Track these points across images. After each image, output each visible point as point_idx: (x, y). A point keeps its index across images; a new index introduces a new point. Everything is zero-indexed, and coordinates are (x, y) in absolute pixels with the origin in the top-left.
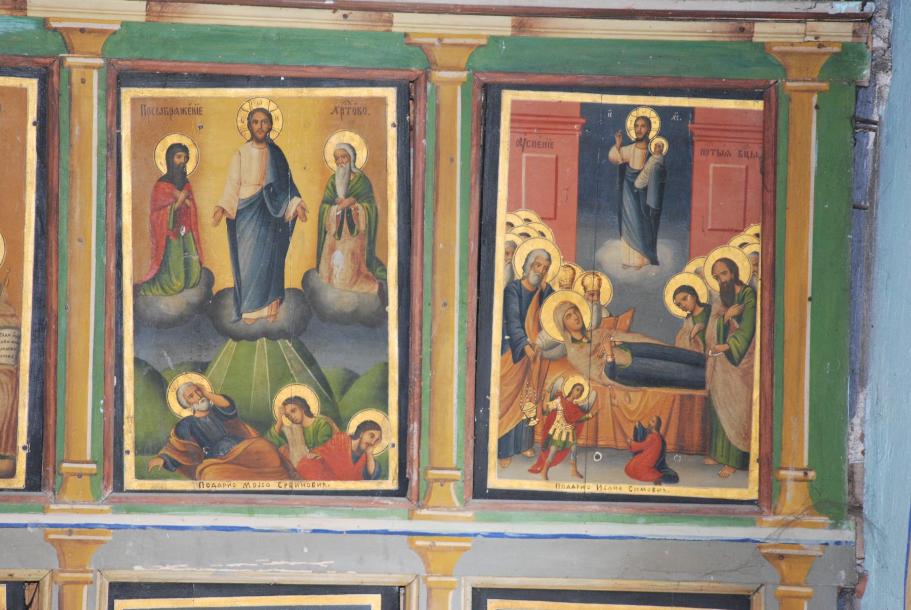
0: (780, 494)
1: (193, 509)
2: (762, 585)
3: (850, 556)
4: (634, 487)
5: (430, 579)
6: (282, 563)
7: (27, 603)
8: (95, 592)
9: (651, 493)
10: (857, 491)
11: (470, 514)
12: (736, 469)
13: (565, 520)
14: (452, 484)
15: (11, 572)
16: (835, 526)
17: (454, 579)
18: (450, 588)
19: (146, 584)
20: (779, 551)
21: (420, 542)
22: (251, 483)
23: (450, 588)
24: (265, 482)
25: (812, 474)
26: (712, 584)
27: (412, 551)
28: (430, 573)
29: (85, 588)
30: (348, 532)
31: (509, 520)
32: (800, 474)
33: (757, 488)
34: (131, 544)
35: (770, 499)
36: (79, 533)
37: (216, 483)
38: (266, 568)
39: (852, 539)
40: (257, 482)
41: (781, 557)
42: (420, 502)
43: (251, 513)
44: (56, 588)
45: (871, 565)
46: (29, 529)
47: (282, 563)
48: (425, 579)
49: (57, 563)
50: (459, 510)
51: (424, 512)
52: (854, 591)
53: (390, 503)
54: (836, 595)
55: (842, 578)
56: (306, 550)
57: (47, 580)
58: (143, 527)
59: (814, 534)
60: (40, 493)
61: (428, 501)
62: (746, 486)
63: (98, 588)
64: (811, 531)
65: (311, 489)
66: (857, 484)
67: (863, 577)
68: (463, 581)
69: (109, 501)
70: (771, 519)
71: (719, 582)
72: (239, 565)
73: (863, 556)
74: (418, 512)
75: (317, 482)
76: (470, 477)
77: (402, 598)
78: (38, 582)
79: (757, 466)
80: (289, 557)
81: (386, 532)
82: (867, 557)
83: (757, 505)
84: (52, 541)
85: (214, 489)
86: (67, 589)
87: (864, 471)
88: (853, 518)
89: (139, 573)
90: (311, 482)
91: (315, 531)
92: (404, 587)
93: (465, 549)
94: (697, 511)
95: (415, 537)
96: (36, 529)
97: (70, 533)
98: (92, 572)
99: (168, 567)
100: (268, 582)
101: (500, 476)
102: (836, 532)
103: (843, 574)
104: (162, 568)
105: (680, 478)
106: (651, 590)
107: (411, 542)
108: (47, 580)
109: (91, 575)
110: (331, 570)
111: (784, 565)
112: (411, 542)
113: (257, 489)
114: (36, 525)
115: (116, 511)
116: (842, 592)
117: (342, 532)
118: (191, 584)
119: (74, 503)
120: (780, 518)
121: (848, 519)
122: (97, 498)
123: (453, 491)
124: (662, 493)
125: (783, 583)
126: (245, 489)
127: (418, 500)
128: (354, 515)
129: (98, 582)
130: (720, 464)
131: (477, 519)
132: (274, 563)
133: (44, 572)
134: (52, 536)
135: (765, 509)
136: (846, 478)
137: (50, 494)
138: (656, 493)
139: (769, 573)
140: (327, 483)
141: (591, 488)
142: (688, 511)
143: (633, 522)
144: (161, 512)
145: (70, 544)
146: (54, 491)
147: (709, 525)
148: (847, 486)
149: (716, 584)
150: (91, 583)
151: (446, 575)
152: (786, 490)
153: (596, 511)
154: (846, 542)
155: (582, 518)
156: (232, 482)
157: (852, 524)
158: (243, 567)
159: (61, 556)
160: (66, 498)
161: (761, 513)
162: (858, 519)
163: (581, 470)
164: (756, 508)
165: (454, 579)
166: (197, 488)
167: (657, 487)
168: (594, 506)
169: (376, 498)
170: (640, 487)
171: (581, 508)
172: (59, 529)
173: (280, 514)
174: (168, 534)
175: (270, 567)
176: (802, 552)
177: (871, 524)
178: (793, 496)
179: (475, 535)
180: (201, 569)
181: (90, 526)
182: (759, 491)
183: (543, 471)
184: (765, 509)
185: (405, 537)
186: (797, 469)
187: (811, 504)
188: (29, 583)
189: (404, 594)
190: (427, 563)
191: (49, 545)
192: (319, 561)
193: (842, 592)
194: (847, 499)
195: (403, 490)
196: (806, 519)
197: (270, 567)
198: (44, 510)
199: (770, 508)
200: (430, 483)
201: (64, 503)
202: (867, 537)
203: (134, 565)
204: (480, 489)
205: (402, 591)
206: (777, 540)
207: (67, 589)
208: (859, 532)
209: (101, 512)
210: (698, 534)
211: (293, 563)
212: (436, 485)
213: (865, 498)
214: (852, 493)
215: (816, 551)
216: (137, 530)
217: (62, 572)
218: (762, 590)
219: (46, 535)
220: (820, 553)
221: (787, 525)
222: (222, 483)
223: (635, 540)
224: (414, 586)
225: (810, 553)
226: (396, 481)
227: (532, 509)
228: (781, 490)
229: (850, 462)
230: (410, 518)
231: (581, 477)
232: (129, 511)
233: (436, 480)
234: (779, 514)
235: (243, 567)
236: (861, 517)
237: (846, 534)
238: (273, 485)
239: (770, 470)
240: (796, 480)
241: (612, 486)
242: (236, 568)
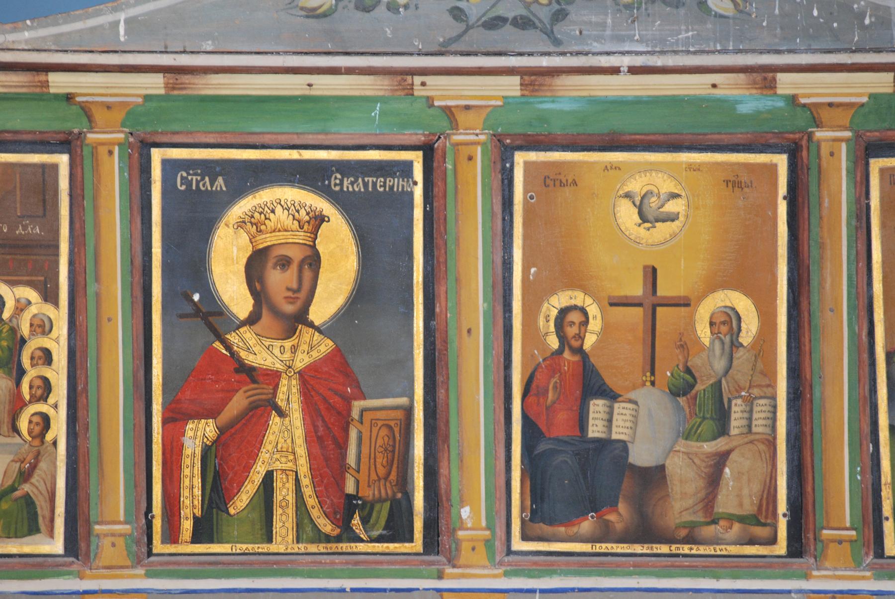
46: (793, 595)
60: (801, 560)
69: (870, 567)
96: (799, 595)
114: (800, 591)
115: (878, 577)
119: (836, 569)
122: (858, 565)
137: (812, 560)
146: (815, 558)
160: (827, 564)
198: (807, 577)
209: (863, 578)
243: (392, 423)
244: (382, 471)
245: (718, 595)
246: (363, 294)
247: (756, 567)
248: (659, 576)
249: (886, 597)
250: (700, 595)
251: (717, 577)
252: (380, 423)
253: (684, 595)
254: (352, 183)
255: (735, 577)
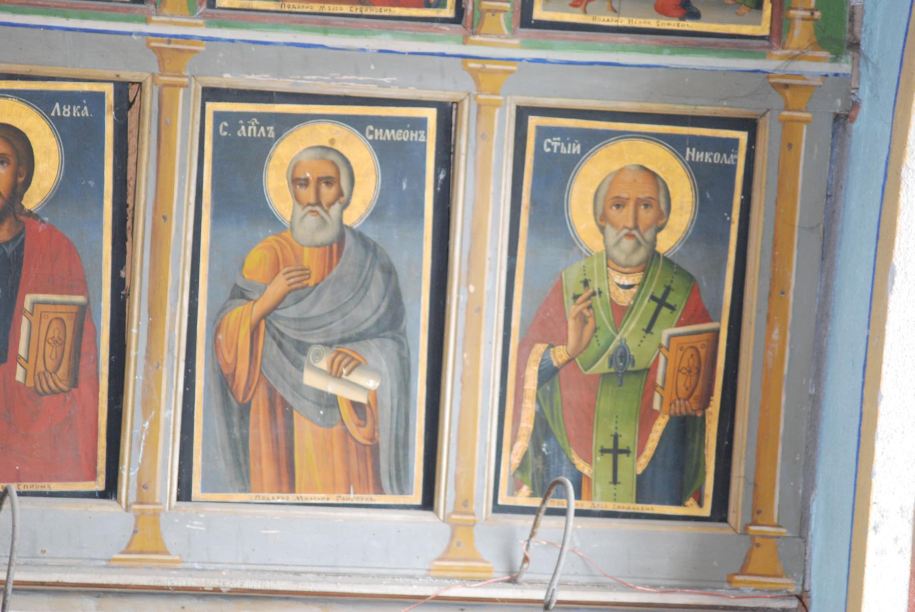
0: (788, 31)
1: (276, 27)
2: (768, 110)
3: (845, 86)
4: (661, 22)
5: (481, 97)
6: (352, 77)
7: (131, 100)
8: (190, 94)
9: (675, 28)
10: (856, 29)
11: (516, 41)
12: (751, 8)
13: (600, 50)
14: (502, 15)
15: (118, 73)
16: (834, 60)
17: (500, 98)
18: (496, 105)
19: (233, 90)
20: (785, 81)
21: (473, 65)
22: (327, 6)
23: (496, 105)
24: (339, 6)
25: (817, 14)
26: (725, 109)
27: (465, 72)
28: (480, 91)
29: (181, 91)
30: (410, 53)
31: (551, 48)
32: (808, 14)
33: (768, 26)
34: (221, 55)
35: (780, 35)
36: (177, 43)
37: (296, 5)
38: (337, 81)
39: (849, 71)
40: (332, 6)
41: (787, 86)
42: (474, 29)
43: (326, 32)
44: (156, 89)
45: (864, 94)
46: (134, 36)
47: (352, 77)
48: (476, 97)
49: (157, 68)
50: (507, 38)
51: (477, 38)
52: (847, 116)
53: (447, 29)
54: (832, 120)
55: (838, 105)
56: (372, 67)
57: (149, 83)
58: (232, 41)
59: (817, 67)
60: (142, 6)
61: (481, 28)
62: (759, 23)
63: (193, 91)
64: (814, 64)
65: (378, 13)
66: (857, 24)
67: (856, 105)
68: (509, 99)
69: (203, 16)
70: (779, 52)
71: (731, 107)
72: (314, 77)
73: (857, 86)
74: (472, 38)
75: (384, 8)
76: (518, 9)
77: (454, 113)
78: (140, 84)
79: (770, 6)
80: (357, 72)
81: (443, 55)
82: (861, 87)
83: (768, 40)
84: (154, 49)
85: (294, 10)
86: (166, 91)
87: (863, 11)
88: (851, 53)
89: (227, 80)
90: (378, 8)
91: (381, 51)
92: (457, 103)
93: (511, 72)
94: (715, 44)
95: (468, 60)
96: (140, 37)
97: (169, 42)
98: (187, 77)
99: (253, 77)
100: (339, 94)
101: (545, 9)
102: (836, 65)
103: (839, 102)
104: (248, 77)
105: (702, 14)
106: (672, 112)
107: (465, 64)
108: (149, 83)
109: (186, 80)
110: (394, 85)
111: (788, 93)
112: (465, 64)
113: (332, 11)
114: (139, 34)
115: (209, 25)
116: (837, 117)
117: (404, 53)
118: (272, 93)
119: (172, 16)
120: (788, 52)
121: (847, 54)
122: (192, 12)
123: (502, 21)
124: (686, 28)
125: (787, 108)
126: (321, 11)
127: (472, 27)
128: (416, 38)
129: (193, 86)
130: (738, 3)
131: (523, 46)
132: (345, 77)
133: (146, 75)
134: (153, 44)
135: (775, 44)
136: (848, 17)
137: (152, 7)
138: (680, 28)
139: (775, 100)
140: (393, 9)
141: (624, 22)
142: (707, 44)
143: (659, 52)
144: (248, 28)
145: (169, 52)
146: (156, 5)
147: (725, 57)
148: (847, 25)
149: (728, 109)
150: (187, 86)
151: (494, 94)
152: (794, 28)
153: (627, 42)
154: (844, 74)
155: (614, 49)
156: (310, 5)
157: (849, 58)
158: (317, 80)
159: (161, 62)
160: (166, 11)
161: (771, 47)
162: (856, 54)
163: (616, 6)
164: (766, 43)
165: (500, 98)
166: (279, 8)
167: (682, 23)
168: (625, 38)
169: (435, 25)
170: (666, 22)
171: (614, 39)
172: (160, 38)
173: (352, 34)
174: (253, 48)
175: (341, 81)
176: (805, 82)
177: (867, 59)
178: (800, 33)
179: (521, 60)
180: (282, 80)
181: (186, 38)
182: (771, 28)
183: (582, 6)
184: (775, 44)
185: (460, 60)
186: (805, 10)
187: (815, 39)
188: (133, 83)
189: (457, 109)
190: (478, 83)
191: (150, 51)
192: (384, 77)
193: (837, 117)
194: (848, 36)
195: (459, 17)
196: (810, 54)
197: (341, 81)
198: (147, 21)
199: (779, 43)
200: (482, 13)
201: (164, 15)
202: (863, 70)
203: (222, 73)
204: (526, 20)
205: (455, 106)
206: (784, 71)
207: (166, 91)
208: (856, 65)
209: (196, 25)
210: (714, 65)
211: (361, 78)
212: (488, 15)
213: (863, 35)
214: (851, 31)
215: (818, 82)
216: (227, 43)
217: (162, 75)
218: (768, 115)
219: (148, 42)
220: (821, 83)
221: (793, 58)
222: (301, 5)
223: (660, 69)
224: (466, 103)
225: (812, 83)
226: (453, 10)
227: (571, 39)
228: (790, 27)
229: (852, 4)
230: (464, 43)
231: (615, 11)
232: (220, 25)
233: (489, 11)
234: (787, 48)
235: (317, 80)
236: (859, 52)
237: (844, 67)
238: (346, 9)
239: (782, 10)
240: (803, 19)
241: (642, 20)
242: (311, 80)
243: (63, 316)
244: (50, 364)
245: (67, 33)
246: (60, 194)
247: (103, 10)
248: (14, 12)
249: (214, 43)
250: (50, 31)
251: (67, 17)
252: (51, 316)
253: (37, 30)
254: (80, 111)
255: (83, 18)
